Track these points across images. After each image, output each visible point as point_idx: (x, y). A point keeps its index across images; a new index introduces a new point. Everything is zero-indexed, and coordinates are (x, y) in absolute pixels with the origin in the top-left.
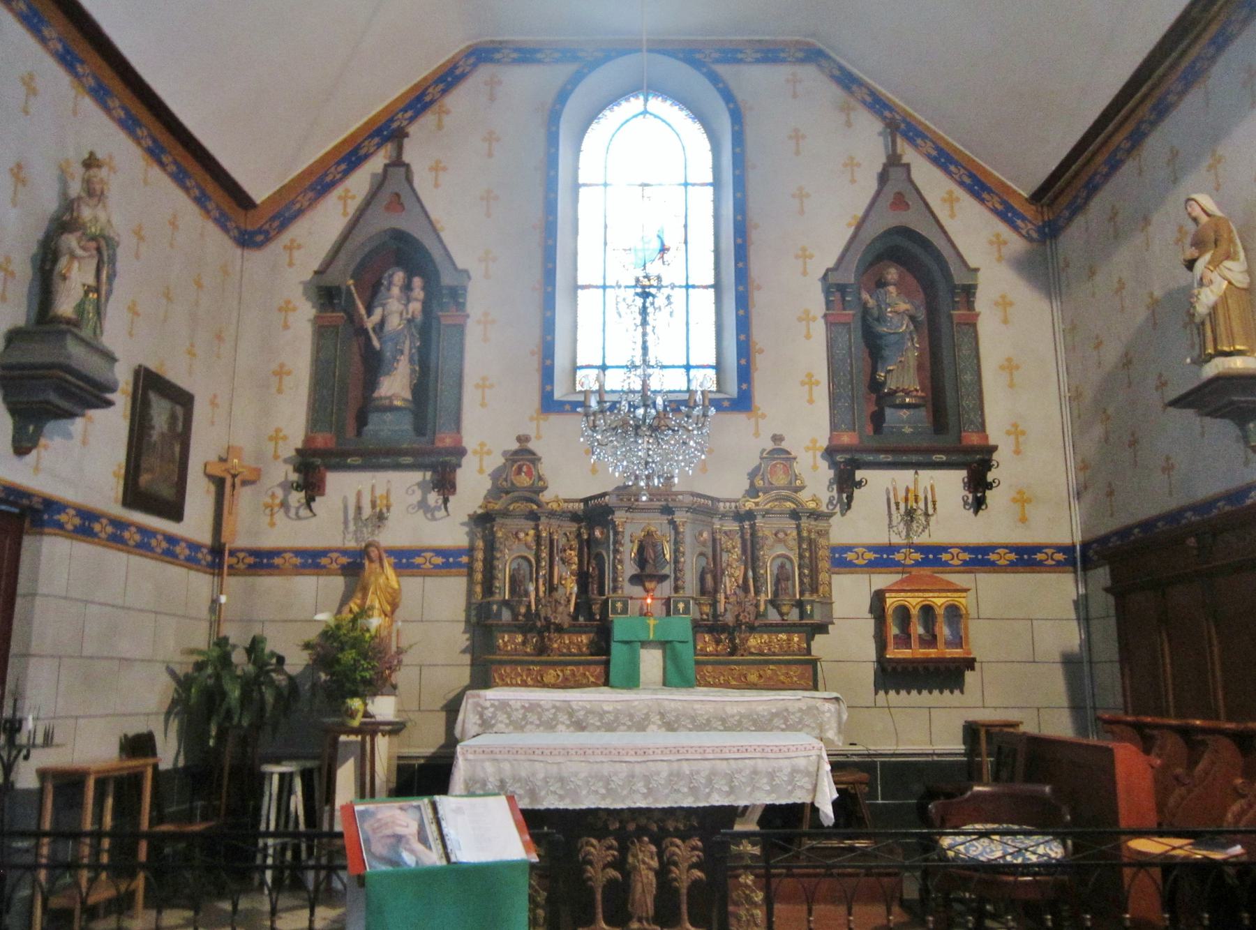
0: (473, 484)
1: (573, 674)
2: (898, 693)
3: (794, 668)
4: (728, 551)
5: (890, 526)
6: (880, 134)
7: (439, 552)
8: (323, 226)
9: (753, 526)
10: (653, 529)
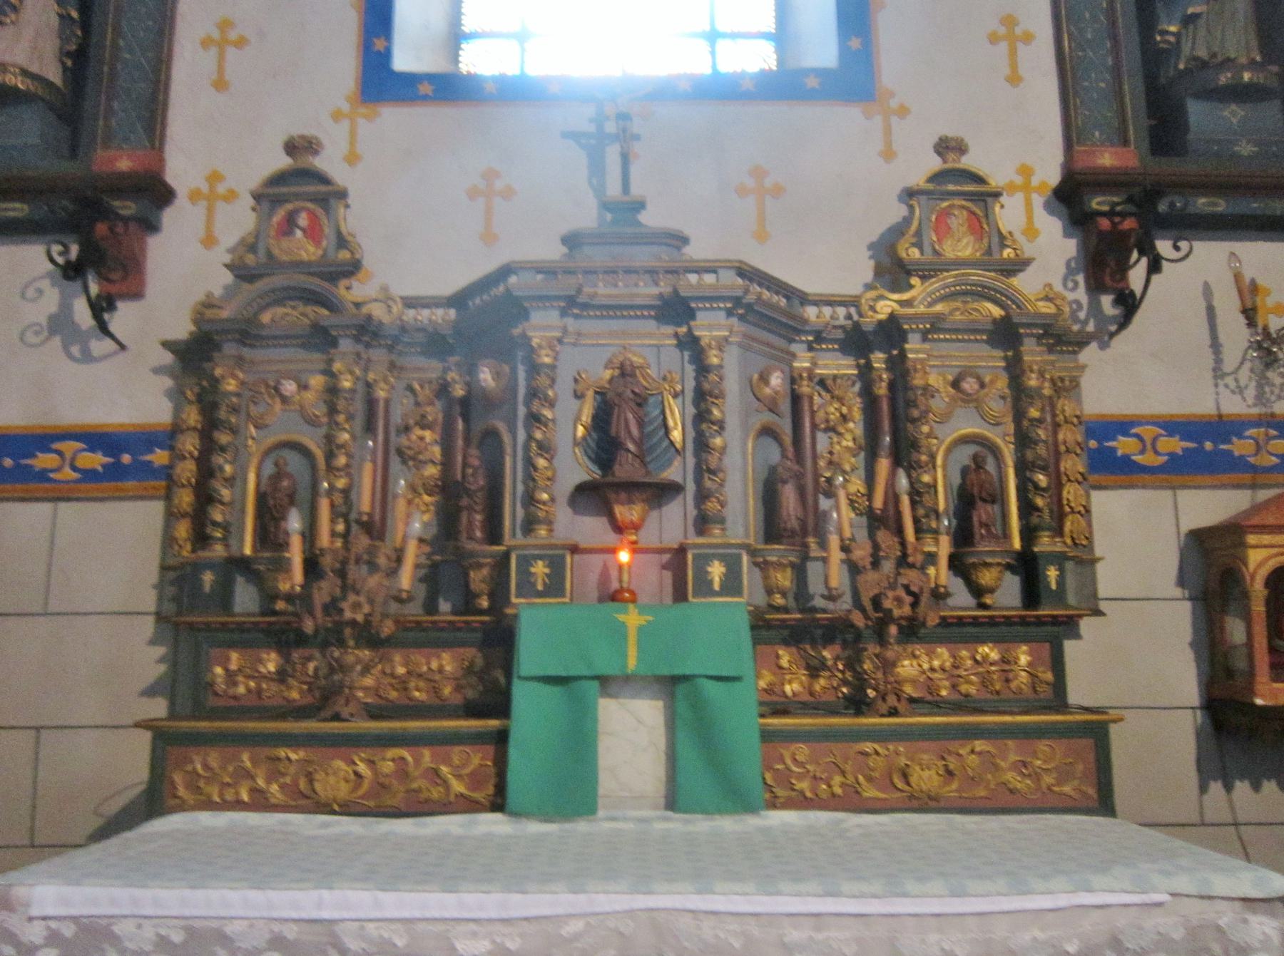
0: (186, 264)
1: (402, 772)
2: (1256, 787)
3: (1043, 746)
4: (831, 429)
5: (1218, 372)
7: (95, 439)
9: (898, 365)
10: (637, 360)
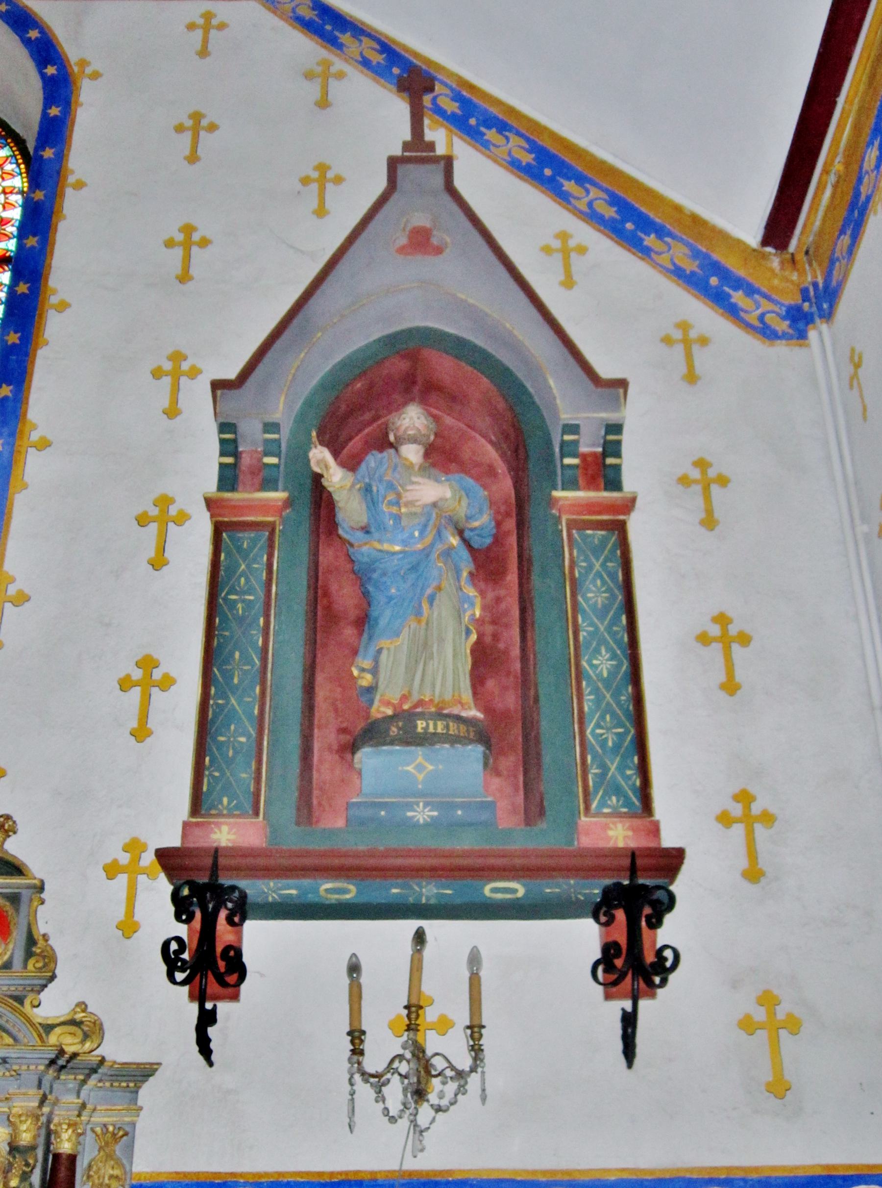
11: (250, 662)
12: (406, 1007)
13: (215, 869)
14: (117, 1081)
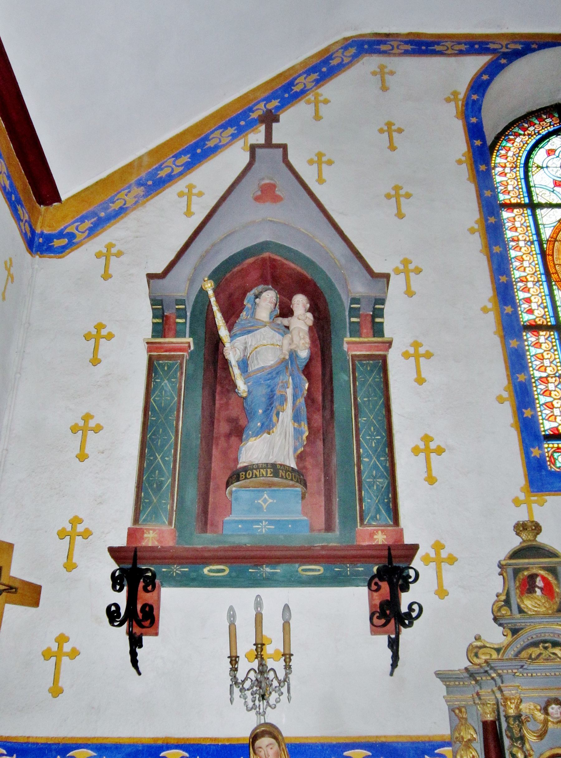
6: (481, 252)
8: (158, 229)
11: (367, 442)
12: (254, 645)
13: (135, 559)
14: (448, 681)
